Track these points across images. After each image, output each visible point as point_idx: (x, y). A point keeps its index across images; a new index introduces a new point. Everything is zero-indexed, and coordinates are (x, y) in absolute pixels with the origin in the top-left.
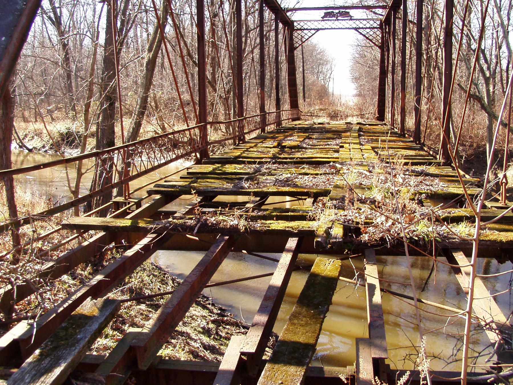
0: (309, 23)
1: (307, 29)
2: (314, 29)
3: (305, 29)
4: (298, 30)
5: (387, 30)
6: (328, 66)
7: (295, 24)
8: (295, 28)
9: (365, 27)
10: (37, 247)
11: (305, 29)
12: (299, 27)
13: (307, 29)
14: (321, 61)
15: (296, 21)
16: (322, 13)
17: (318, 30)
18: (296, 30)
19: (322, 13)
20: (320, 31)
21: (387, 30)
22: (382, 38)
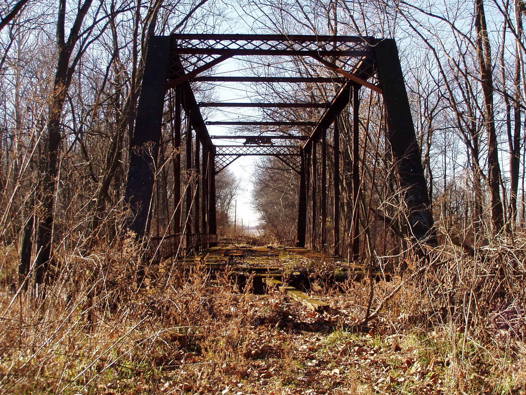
0: (231, 149)
1: (229, 154)
2: (235, 154)
3: (227, 154)
4: (220, 154)
5: (307, 157)
6: (227, 190)
7: (217, 149)
8: (217, 153)
9: (231, 153)
10: (303, 267)
11: (227, 154)
12: (221, 152)
13: (229, 154)
14: (229, 184)
15: (218, 146)
16: (244, 140)
17: (240, 155)
18: (218, 154)
19: (244, 140)
20: (242, 156)
21: (307, 157)
22: (302, 165)
